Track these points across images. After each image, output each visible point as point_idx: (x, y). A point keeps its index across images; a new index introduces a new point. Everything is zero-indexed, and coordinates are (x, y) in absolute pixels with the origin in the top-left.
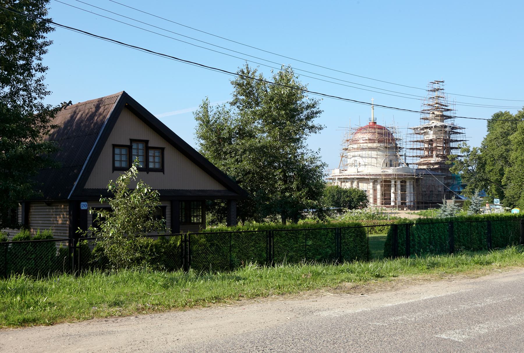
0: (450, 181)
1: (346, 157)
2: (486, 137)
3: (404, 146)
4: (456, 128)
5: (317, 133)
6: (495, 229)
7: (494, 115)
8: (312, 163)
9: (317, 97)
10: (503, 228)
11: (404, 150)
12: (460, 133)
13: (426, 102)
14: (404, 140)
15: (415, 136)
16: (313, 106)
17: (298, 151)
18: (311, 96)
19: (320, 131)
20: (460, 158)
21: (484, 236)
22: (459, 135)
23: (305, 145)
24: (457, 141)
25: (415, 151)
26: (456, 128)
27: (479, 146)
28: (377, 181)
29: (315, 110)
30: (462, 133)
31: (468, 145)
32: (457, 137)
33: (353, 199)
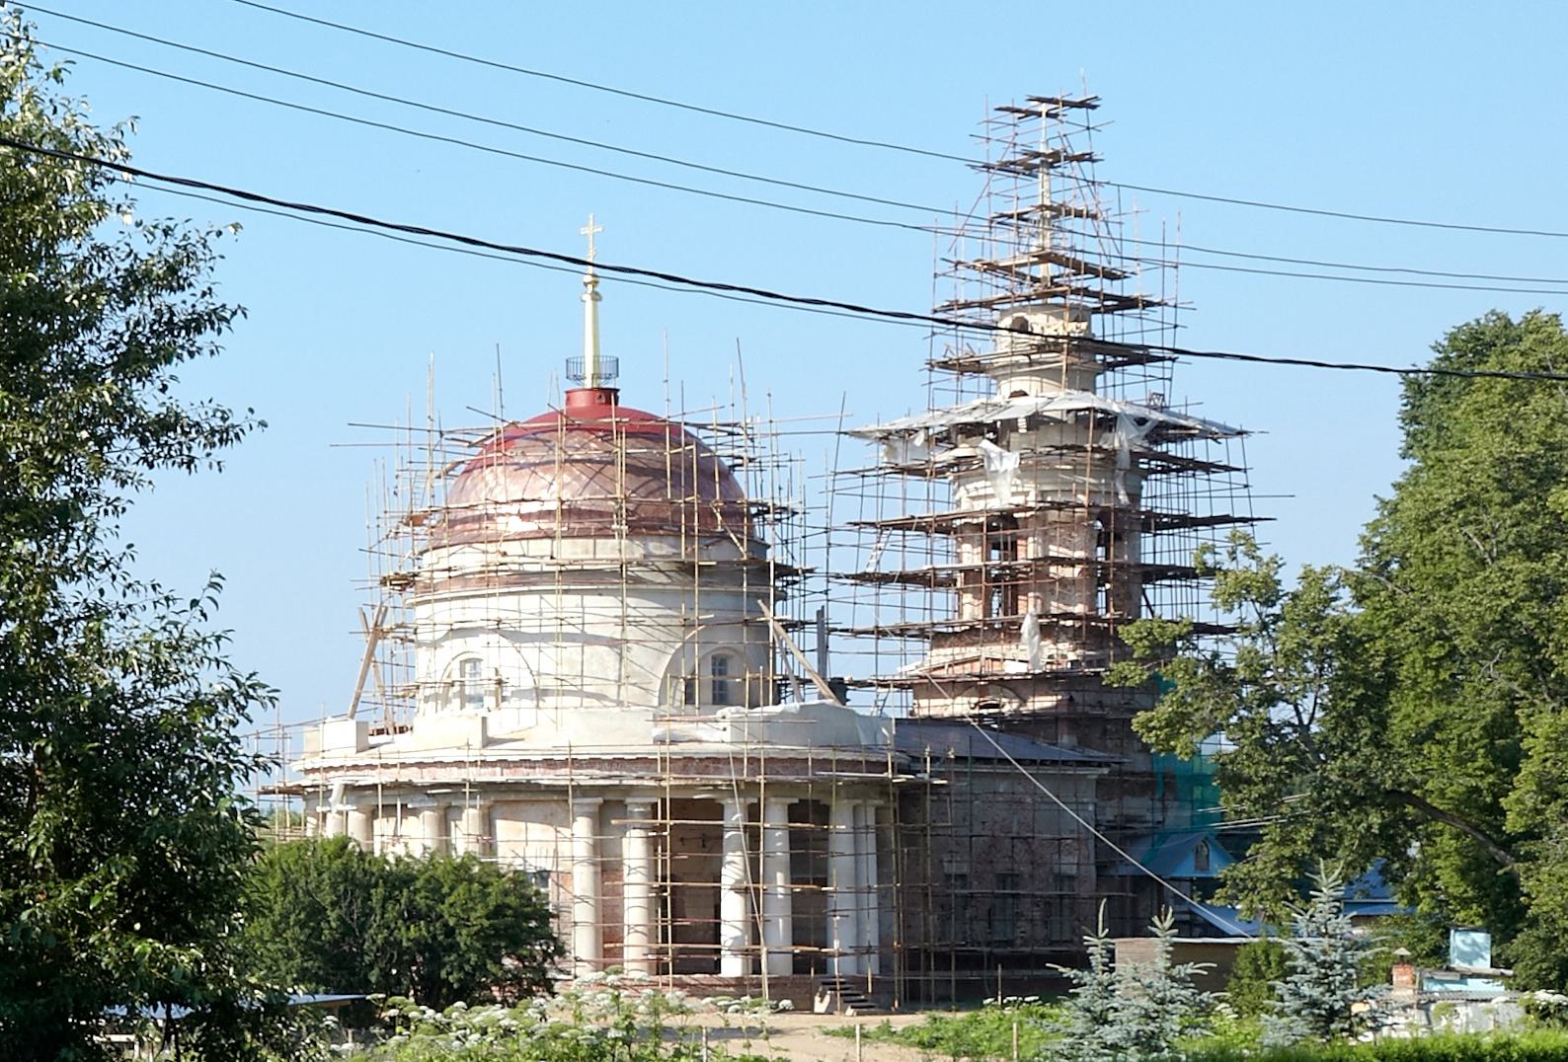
0: (1136, 806)
2: (1391, 495)
3: (814, 559)
4: (1184, 434)
5: (201, 464)
7: (1452, 338)
9: (195, 215)
11: (815, 583)
12: (1207, 467)
13: (969, 251)
14: (817, 519)
15: (895, 485)
17: (67, 590)
18: (157, 204)
19: (219, 452)
20: (1207, 644)
22: (1200, 482)
24: (1186, 522)
25: (892, 593)
26: (1184, 434)
27: (1348, 556)
28: (622, 804)
29: (181, 302)
30: (1227, 469)
31: (1265, 554)
32: (1186, 495)
33: (450, 932)
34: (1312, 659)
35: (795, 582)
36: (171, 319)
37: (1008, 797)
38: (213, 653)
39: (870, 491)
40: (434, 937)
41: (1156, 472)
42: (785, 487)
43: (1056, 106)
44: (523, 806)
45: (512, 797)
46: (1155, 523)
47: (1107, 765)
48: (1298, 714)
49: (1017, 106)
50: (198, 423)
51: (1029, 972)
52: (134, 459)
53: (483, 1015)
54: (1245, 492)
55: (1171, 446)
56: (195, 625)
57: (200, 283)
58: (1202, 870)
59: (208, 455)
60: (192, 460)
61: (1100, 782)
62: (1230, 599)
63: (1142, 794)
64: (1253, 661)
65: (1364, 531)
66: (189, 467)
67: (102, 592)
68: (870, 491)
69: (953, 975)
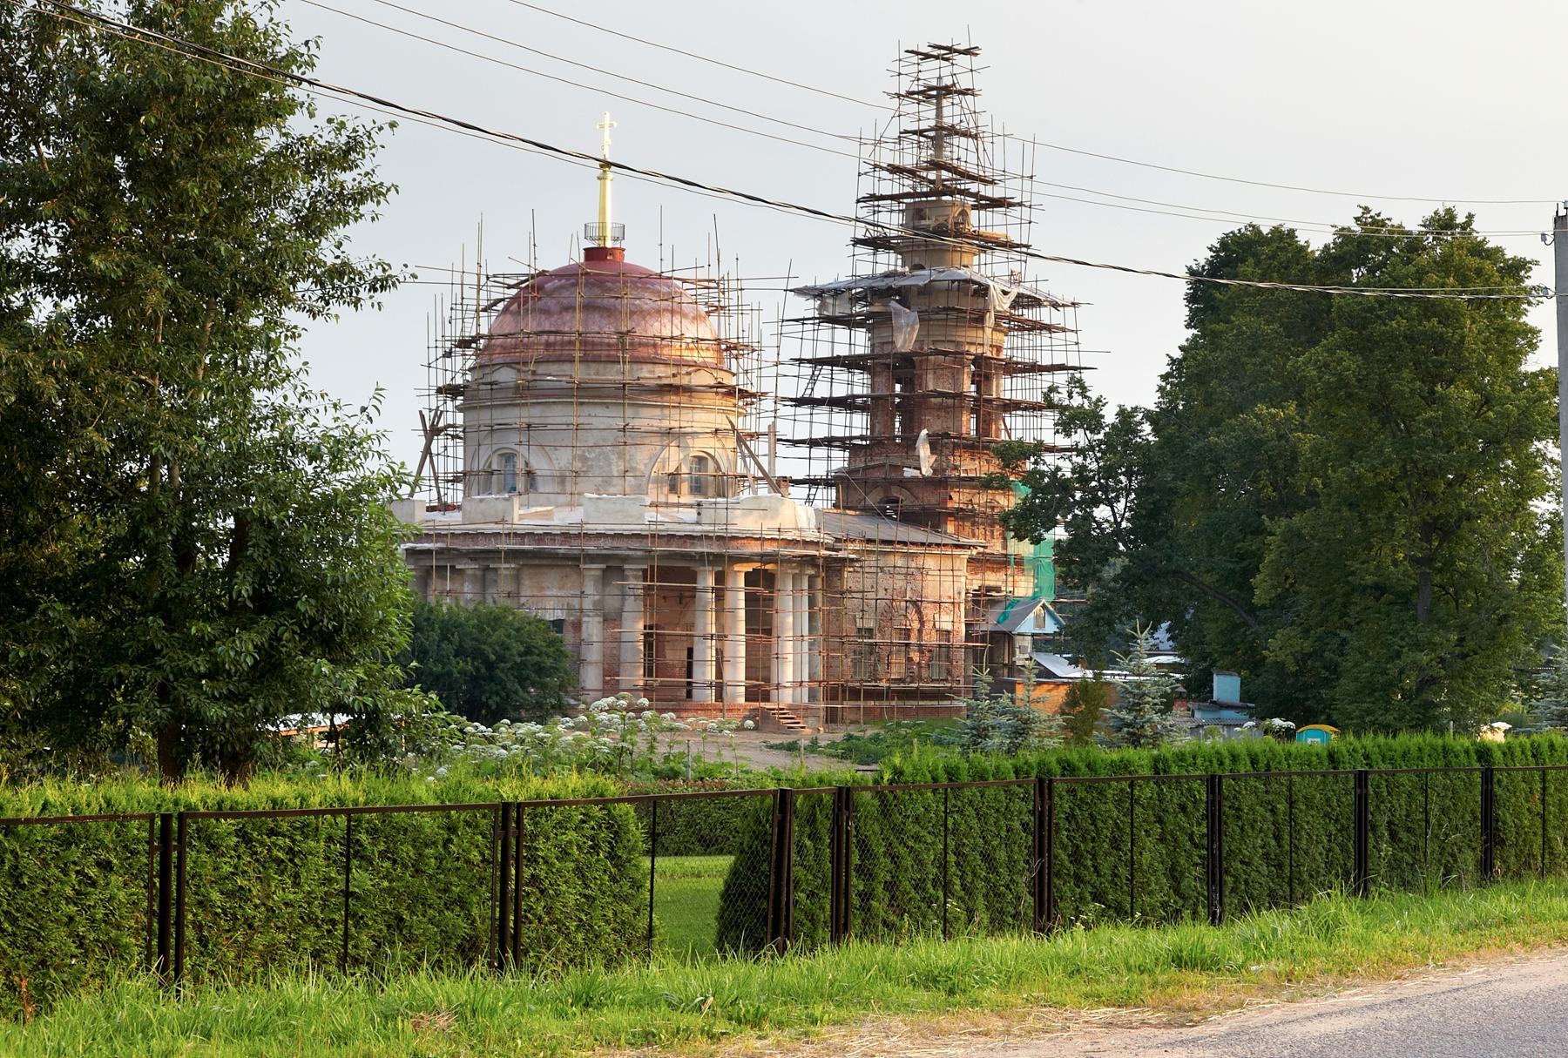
0: (992, 579)
1: (450, 431)
2: (1178, 354)
3: (767, 386)
4: (1035, 302)
5: (366, 304)
6: (1239, 818)
7: (1223, 242)
8: (336, 464)
9: (361, 116)
10: (1273, 811)
11: (768, 404)
12: (1049, 328)
13: (887, 157)
14: (769, 355)
15: (825, 331)
16: (345, 156)
17: (258, 395)
18: (328, 106)
19: (379, 296)
20: (1050, 459)
21: (1190, 856)
22: (1044, 338)
23: (294, 369)
24: (1035, 368)
25: (822, 414)
26: (1035, 302)
27: (1150, 400)
28: (621, 570)
29: (348, 178)
30: (1064, 330)
31: (1093, 395)
32: (1034, 348)
33: (490, 666)
34: (1123, 474)
35: (752, 403)
36: (341, 192)
37: (904, 571)
38: (375, 447)
39: (808, 335)
40: (478, 670)
41: (1014, 330)
42: (746, 329)
43: (947, 53)
44: (546, 570)
45: (537, 562)
46: (1012, 368)
47: (975, 547)
48: (1114, 514)
49: (920, 50)
50: (360, 272)
51: (915, 703)
52: (314, 298)
53: (524, 728)
54: (1076, 348)
55: (1025, 311)
56: (363, 425)
57: (366, 165)
58: (1040, 627)
59: (371, 297)
60: (359, 300)
61: (971, 560)
62: (1066, 427)
63: (999, 570)
64: (1080, 470)
65: (1160, 382)
66: (356, 306)
67: (285, 398)
68: (808, 335)
69: (862, 704)
